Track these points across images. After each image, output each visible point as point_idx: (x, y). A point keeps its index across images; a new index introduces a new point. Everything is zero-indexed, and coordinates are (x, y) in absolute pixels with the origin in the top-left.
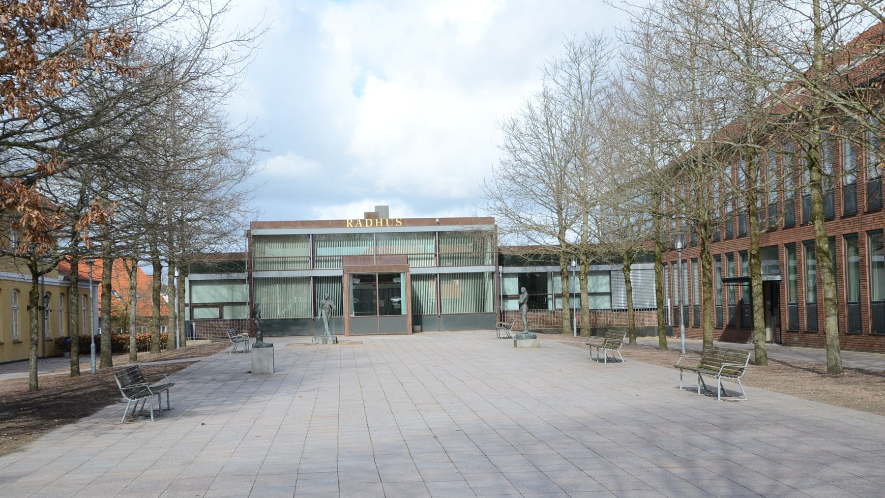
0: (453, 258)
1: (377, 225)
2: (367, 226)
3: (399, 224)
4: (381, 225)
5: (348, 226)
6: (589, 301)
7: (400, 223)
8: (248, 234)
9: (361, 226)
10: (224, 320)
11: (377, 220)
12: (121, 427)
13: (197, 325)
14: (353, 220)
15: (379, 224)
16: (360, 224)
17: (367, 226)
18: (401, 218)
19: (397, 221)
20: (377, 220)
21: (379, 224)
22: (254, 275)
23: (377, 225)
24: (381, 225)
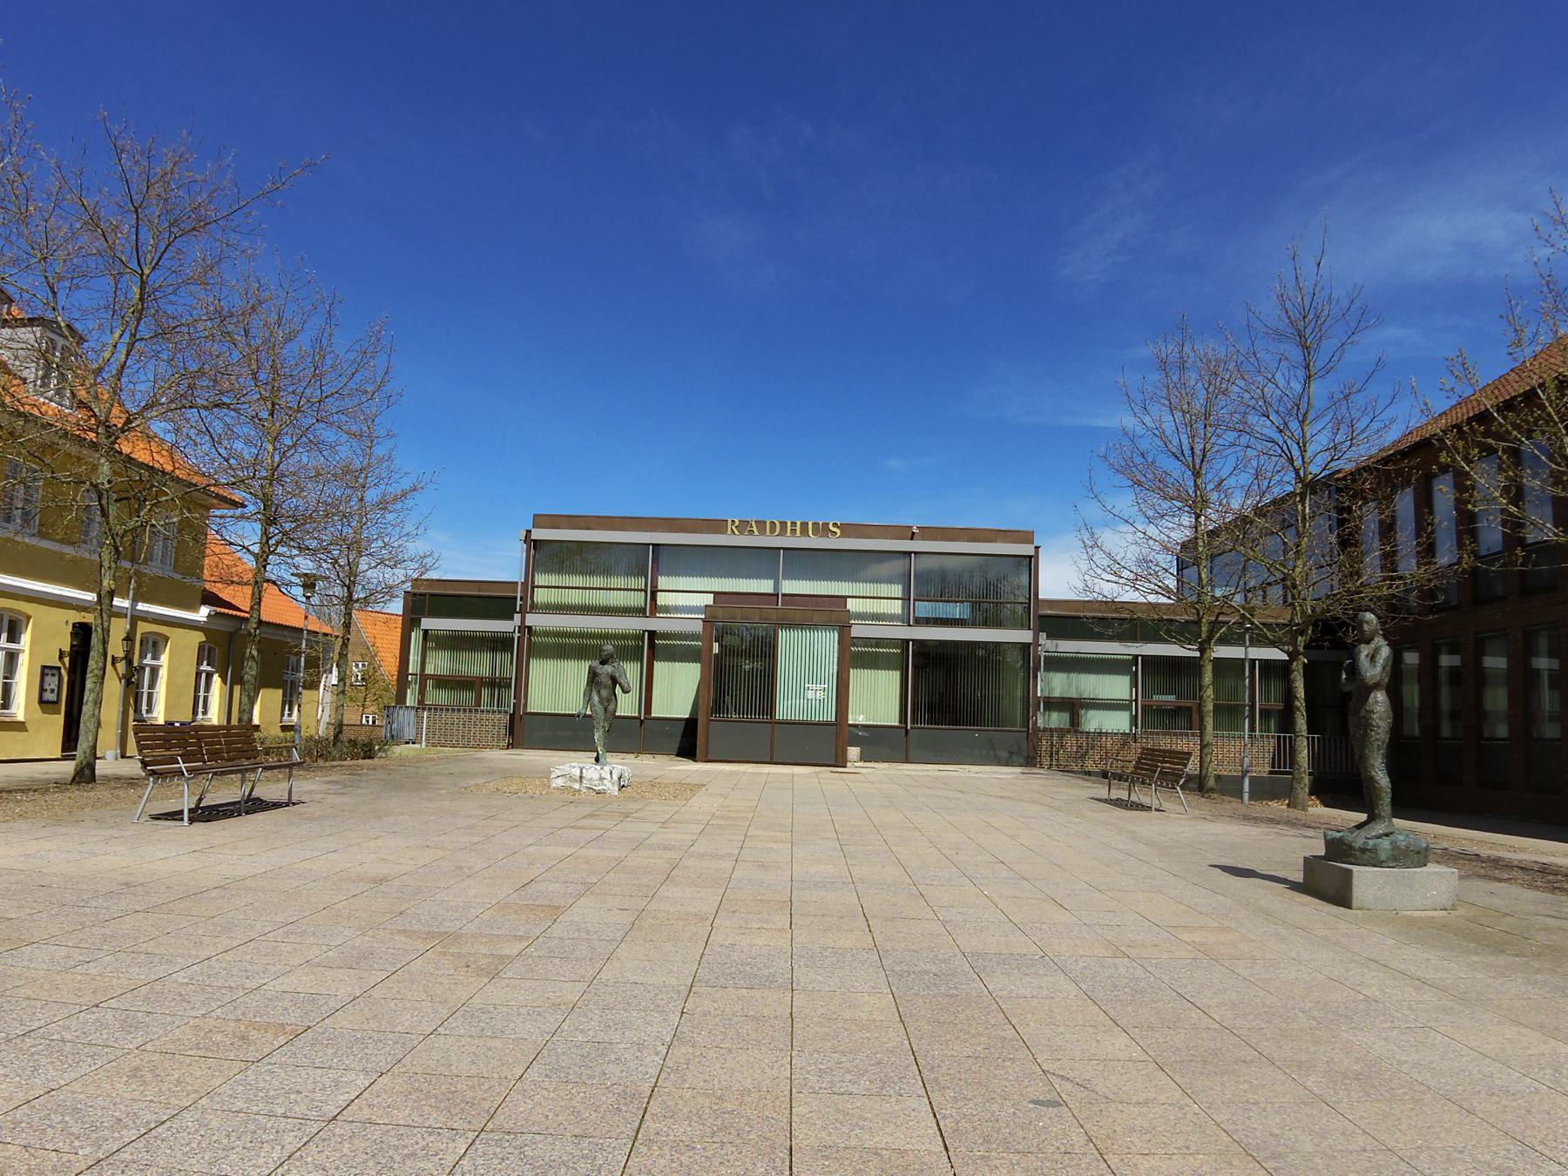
9: (756, 533)
16: (755, 529)
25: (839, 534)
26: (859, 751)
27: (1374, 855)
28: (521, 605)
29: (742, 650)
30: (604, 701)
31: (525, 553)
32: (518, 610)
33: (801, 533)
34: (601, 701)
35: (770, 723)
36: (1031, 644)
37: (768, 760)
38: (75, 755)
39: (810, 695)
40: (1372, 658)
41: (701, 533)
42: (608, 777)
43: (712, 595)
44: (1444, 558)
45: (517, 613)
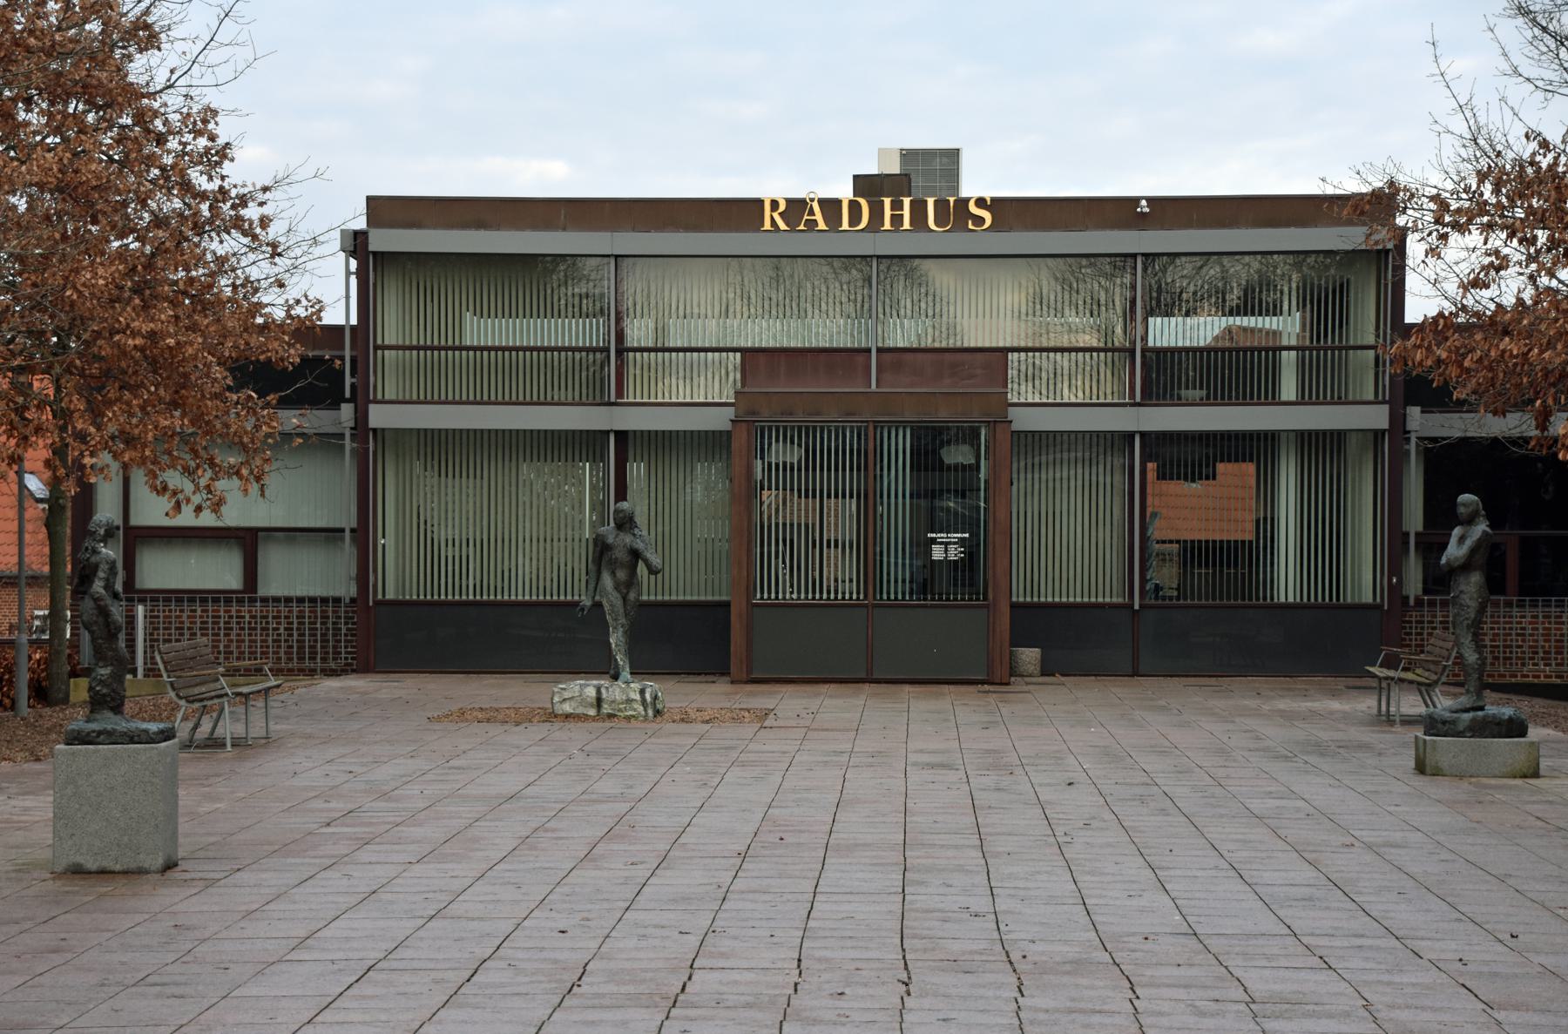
1: (887, 226)
2: (845, 226)
3: (981, 220)
4: (907, 225)
5: (767, 225)
6: (555, 996)
7: (986, 215)
8: (356, 244)
9: (822, 226)
10: (265, 600)
11: (887, 201)
12: (242, 925)
13: (151, 618)
14: (789, 201)
15: (896, 220)
16: (818, 217)
17: (845, 226)
18: (988, 194)
19: (973, 209)
20: (887, 201)
21: (896, 220)
22: (378, 417)
23: (887, 226)
24: (907, 225)
25: (988, 223)
26: (1039, 656)
27: (1452, 727)
28: (353, 385)
29: (807, 496)
30: (622, 587)
31: (353, 280)
32: (348, 394)
33: (911, 224)
34: (617, 588)
35: (866, 606)
36: (1383, 431)
37: (863, 675)
39: (937, 553)
41: (711, 230)
42: (638, 697)
43: (738, 355)
45: (348, 401)
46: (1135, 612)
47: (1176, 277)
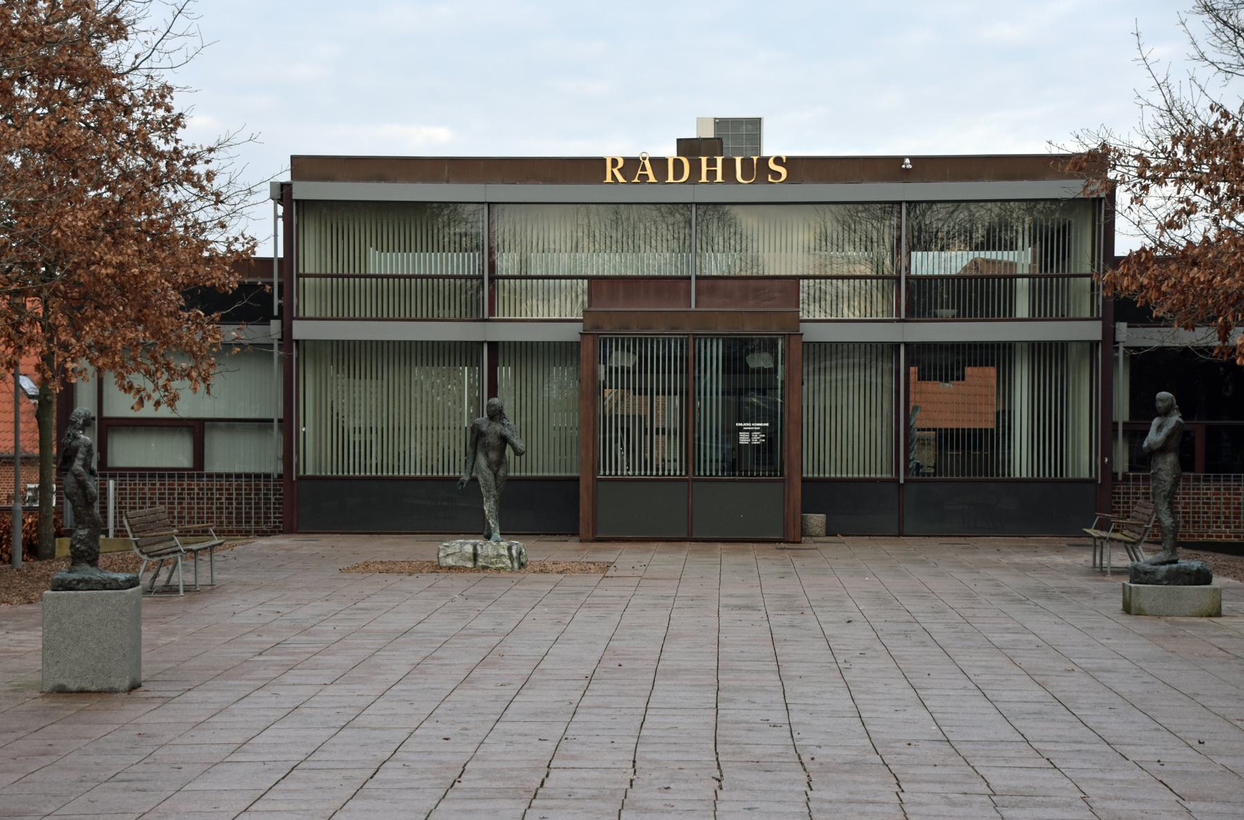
0: (957, 783)
1: (704, 179)
2: (671, 179)
3: (778, 175)
4: (719, 178)
5: (609, 179)
7: (783, 171)
8: (282, 193)
9: (652, 179)
10: (210, 476)
11: (704, 160)
13: (120, 490)
14: (626, 159)
15: (711, 175)
16: (649, 172)
17: (671, 179)
18: (784, 154)
19: (772, 165)
20: (704, 160)
21: (711, 175)
22: (300, 330)
23: (704, 179)
24: (719, 178)
25: (784, 176)
26: (824, 520)
27: (1152, 576)
28: (280, 306)
29: (640, 394)
30: (493, 466)
31: (280, 222)
32: (276, 313)
33: (723, 177)
34: (489, 466)
35: (687, 481)
36: (1098, 342)
37: (685, 536)
38: (1240, 476)
39: (744, 439)
40: (1160, 428)
41: (564, 182)
42: (506, 553)
43: (586, 282)
44: (918, 433)
45: (276, 318)
46: (901, 485)
47: (933, 220)
